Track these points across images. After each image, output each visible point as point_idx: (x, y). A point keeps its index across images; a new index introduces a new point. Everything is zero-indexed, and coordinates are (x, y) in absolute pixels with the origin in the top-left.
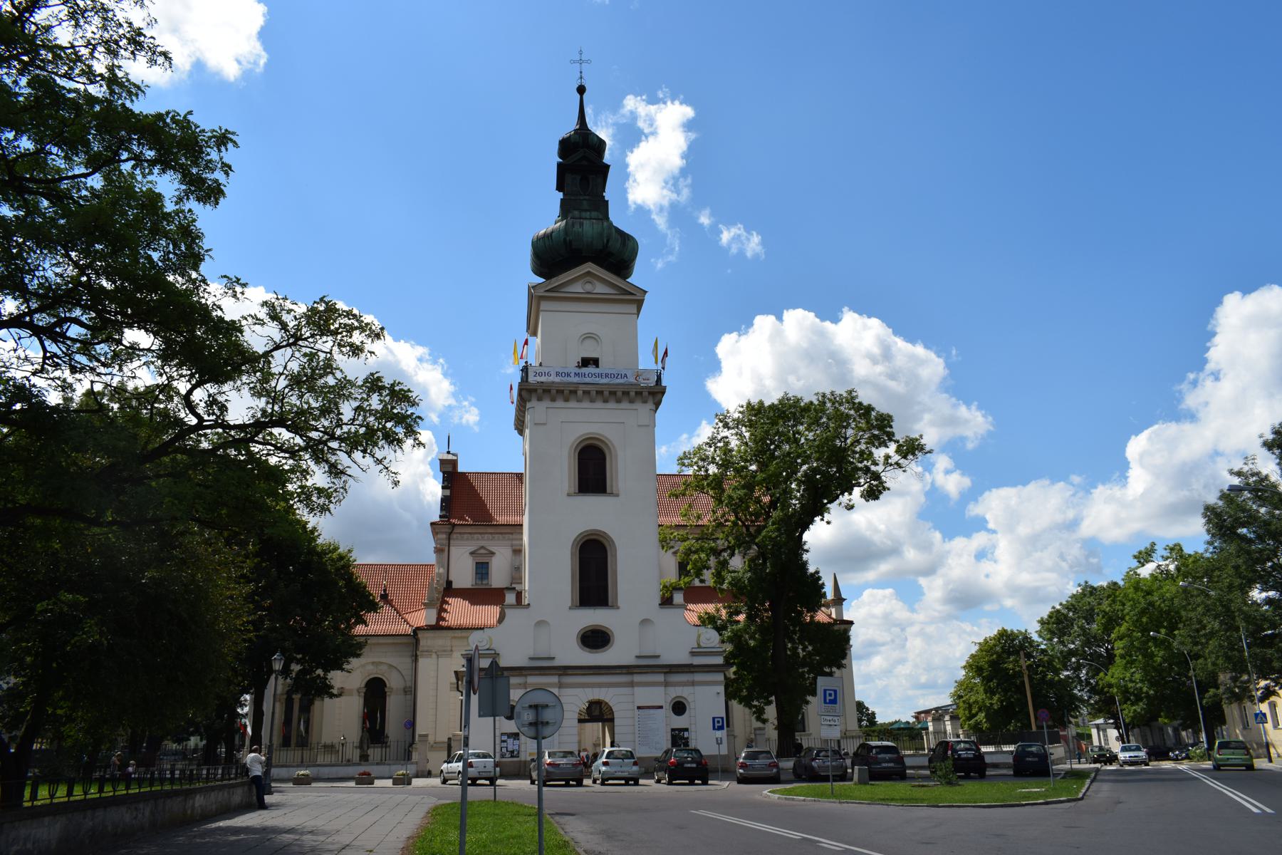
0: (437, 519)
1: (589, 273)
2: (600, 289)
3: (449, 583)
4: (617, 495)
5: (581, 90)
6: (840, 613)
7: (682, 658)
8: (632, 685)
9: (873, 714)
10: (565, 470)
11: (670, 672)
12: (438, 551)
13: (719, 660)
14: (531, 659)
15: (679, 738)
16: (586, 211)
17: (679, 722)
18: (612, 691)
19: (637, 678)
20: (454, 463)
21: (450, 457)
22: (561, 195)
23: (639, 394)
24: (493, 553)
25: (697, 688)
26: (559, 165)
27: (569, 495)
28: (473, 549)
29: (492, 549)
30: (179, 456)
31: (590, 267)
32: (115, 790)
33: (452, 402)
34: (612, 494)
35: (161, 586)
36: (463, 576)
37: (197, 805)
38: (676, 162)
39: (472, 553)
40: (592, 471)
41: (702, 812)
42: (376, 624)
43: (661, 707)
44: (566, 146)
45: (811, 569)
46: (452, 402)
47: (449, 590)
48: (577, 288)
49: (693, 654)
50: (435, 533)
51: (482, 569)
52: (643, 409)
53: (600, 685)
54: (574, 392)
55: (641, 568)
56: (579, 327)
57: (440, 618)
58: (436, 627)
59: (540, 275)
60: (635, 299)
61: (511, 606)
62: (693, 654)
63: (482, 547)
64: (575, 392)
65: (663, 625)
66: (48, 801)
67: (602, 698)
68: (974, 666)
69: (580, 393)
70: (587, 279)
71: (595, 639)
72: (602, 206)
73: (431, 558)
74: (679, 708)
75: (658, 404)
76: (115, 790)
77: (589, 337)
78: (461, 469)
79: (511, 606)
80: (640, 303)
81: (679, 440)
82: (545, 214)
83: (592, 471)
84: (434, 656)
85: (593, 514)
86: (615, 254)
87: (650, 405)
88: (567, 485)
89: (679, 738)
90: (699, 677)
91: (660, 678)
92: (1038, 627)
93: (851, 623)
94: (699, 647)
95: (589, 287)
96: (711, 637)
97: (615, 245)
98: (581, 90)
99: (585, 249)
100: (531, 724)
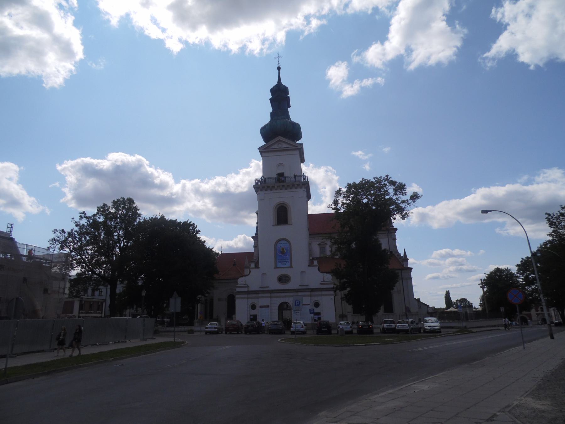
2: (285, 146)
5: (279, 68)
13: (332, 286)
19: (260, 295)
31: (280, 138)
33: (338, 199)
34: (289, 224)
38: (147, 33)
39: (319, 244)
43: (261, 307)
44: (273, 91)
46: (338, 199)
48: (276, 146)
49: (321, 284)
53: (286, 296)
54: (293, 185)
60: (300, 149)
61: (253, 268)
62: (321, 284)
64: (274, 187)
69: (276, 187)
71: (283, 279)
74: (317, 305)
77: (280, 165)
79: (253, 268)
82: (264, 114)
85: (283, 231)
92: (516, 268)
93: (412, 269)
94: (324, 281)
95: (280, 146)
98: (279, 68)
99: (281, 135)
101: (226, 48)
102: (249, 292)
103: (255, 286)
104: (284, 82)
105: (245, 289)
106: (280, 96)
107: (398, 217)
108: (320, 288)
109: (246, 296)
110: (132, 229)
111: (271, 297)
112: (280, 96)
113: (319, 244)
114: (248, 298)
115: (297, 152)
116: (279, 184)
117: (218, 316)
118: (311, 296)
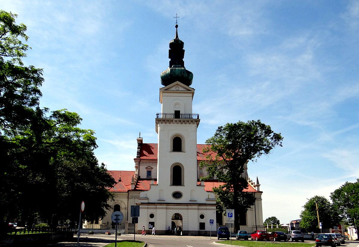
0: (136, 158)
1: (177, 84)
2: (181, 89)
3: (139, 177)
4: (185, 152)
5: (177, 21)
6: (258, 189)
7: (203, 201)
8: (188, 209)
9: (279, 221)
10: (169, 145)
11: (200, 206)
12: (136, 167)
13: (215, 203)
14: (191, 201)
15: (202, 225)
16: (177, 65)
17: (202, 221)
18: (184, 211)
19: (189, 207)
20: (142, 141)
21: (140, 139)
22: (170, 60)
23: (192, 121)
24: (152, 168)
25: (208, 211)
26: (170, 51)
27: (170, 152)
28: (146, 167)
29: (152, 167)
30: (25, 136)
31: (178, 82)
32: (29, 233)
35: (55, 175)
36: (144, 175)
37: (53, 237)
39: (146, 168)
40: (177, 144)
41: (29, 120)
42: (116, 188)
44: (171, 45)
45: (357, 181)
47: (139, 179)
49: (207, 200)
50: (135, 162)
51: (149, 173)
52: (194, 126)
55: (190, 174)
56: (177, 101)
57: (136, 187)
58: (135, 190)
59: (163, 85)
60: (192, 92)
63: (149, 166)
65: (201, 191)
66: (24, 234)
67: (179, 213)
68: (306, 207)
69: (174, 121)
70: (178, 85)
72: (182, 64)
73: (134, 169)
74: (152, 216)
75: (198, 125)
76: (29, 233)
77: (177, 104)
78: (144, 143)
80: (193, 94)
81: (205, 134)
83: (177, 144)
84: (133, 198)
86: (186, 78)
87: (195, 125)
88: (169, 148)
89: (202, 225)
90: (208, 207)
91: (196, 207)
95: (177, 88)
96: (213, 196)
97: (186, 75)
98: (177, 26)
99: (178, 77)
100: (115, 219)
101: (279, 144)
102: (149, 204)
103: (153, 199)
104: (180, 38)
105: (146, 201)
106: (177, 51)
107: (110, 199)
108: (206, 204)
109: (146, 206)
110: (9, 151)
111: (167, 208)
112: (177, 51)
113: (146, 168)
114: (148, 208)
115: (191, 95)
116: (176, 119)
117: (272, 148)
118: (198, 209)
